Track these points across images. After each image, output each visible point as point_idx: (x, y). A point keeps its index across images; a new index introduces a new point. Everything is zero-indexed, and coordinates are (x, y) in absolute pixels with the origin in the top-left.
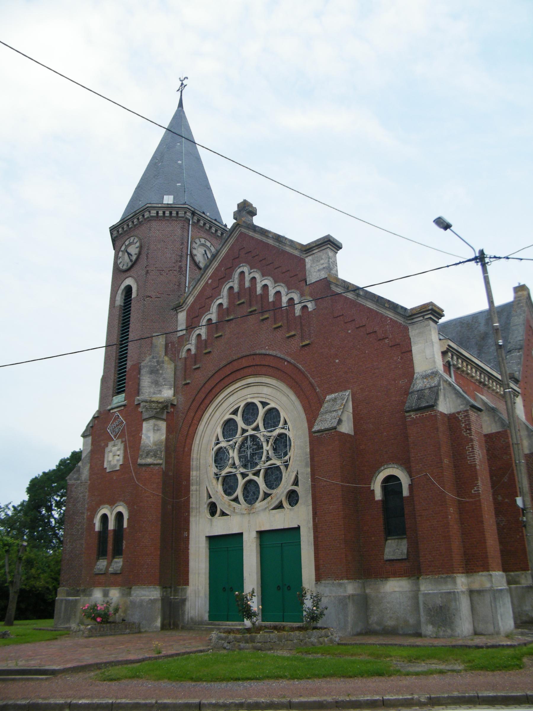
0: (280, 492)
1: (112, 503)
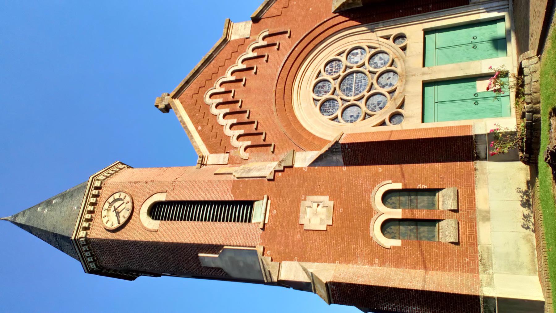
1: (369, 213)
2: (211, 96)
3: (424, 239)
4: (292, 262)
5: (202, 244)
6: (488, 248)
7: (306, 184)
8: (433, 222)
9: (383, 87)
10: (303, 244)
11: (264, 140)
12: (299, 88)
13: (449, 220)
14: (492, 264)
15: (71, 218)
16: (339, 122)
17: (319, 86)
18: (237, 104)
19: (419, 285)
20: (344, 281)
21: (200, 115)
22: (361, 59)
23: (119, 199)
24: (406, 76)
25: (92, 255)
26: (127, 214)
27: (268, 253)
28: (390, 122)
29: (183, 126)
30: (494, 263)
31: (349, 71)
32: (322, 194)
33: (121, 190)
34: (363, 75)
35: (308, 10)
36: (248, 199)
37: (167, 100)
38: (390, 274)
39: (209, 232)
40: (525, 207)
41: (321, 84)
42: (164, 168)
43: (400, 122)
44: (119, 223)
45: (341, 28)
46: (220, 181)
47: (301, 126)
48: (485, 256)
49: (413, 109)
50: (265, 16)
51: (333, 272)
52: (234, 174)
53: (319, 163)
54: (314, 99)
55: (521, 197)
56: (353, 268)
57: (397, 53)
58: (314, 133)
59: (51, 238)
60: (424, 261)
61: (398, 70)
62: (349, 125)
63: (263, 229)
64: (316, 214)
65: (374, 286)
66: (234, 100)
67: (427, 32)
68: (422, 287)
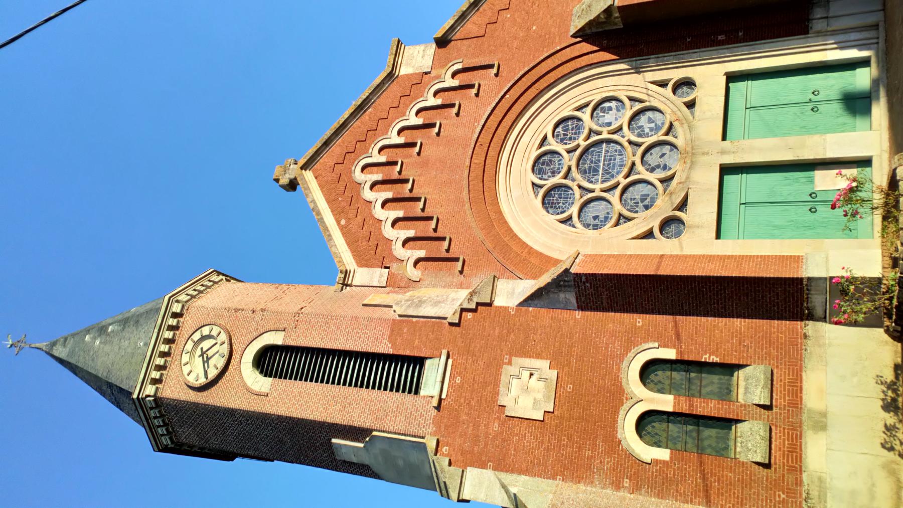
0: (650, 219)
1: (617, 396)
2: (363, 169)
4: (484, 471)
6: (820, 479)
7: (512, 336)
8: (727, 423)
9: (652, 170)
11: (448, 251)
12: (509, 163)
13: (755, 422)
15: (134, 360)
16: (574, 226)
17: (543, 162)
18: (405, 185)
21: (345, 199)
22: (616, 119)
23: (209, 337)
24: (693, 154)
25: (165, 424)
26: (221, 363)
27: (444, 450)
28: (661, 233)
31: (595, 138)
32: (538, 356)
34: (619, 147)
35: (529, 29)
36: (416, 353)
37: (293, 171)
39: (349, 404)
40: (889, 412)
41: (546, 158)
42: (284, 287)
43: (678, 235)
45: (584, 64)
46: (370, 319)
47: (510, 230)
48: (814, 493)
49: (701, 212)
50: (457, 36)
52: (394, 308)
53: (536, 302)
54: (533, 184)
55: (883, 392)
57: (679, 113)
58: (530, 243)
59: (104, 388)
61: (680, 142)
62: (591, 233)
63: (438, 408)
64: (526, 390)
66: (401, 177)
67: (732, 78)
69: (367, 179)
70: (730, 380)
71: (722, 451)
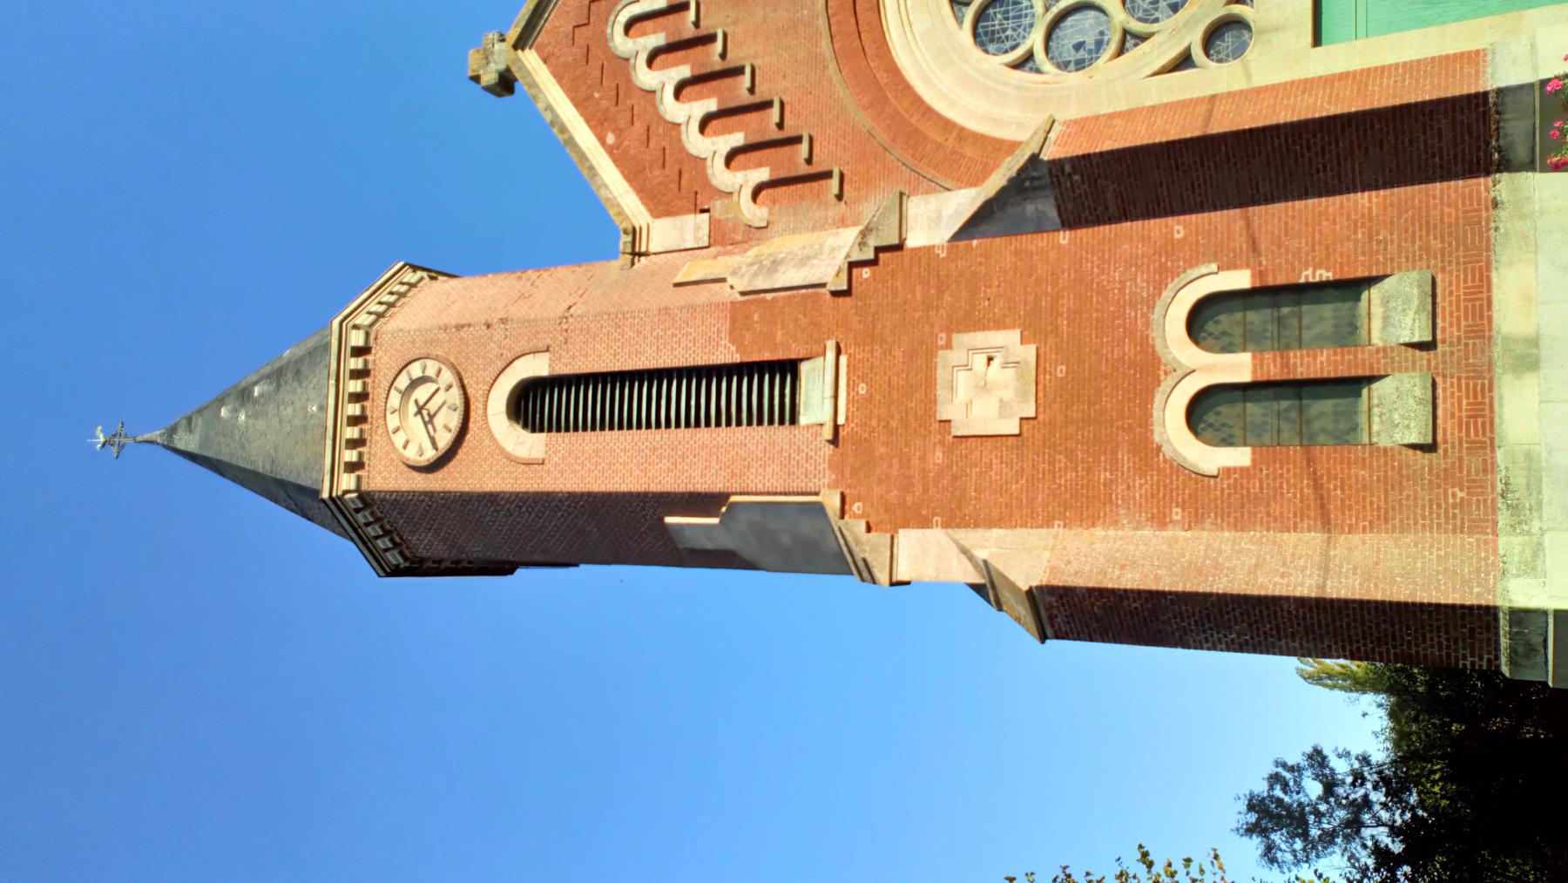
1: (1148, 370)
2: (628, 27)
3: (1321, 438)
4: (928, 531)
5: (668, 494)
6: (1528, 456)
7: (947, 298)
10: (955, 478)
13: (1405, 376)
14: (1540, 504)
15: (309, 438)
16: (1038, 71)
19: (1308, 582)
20: (1080, 582)
26: (455, 421)
27: (855, 507)
28: (1207, 54)
29: (560, 137)
30: (1545, 498)
32: (999, 325)
33: (423, 352)
37: (502, 55)
38: (1220, 552)
39: (683, 457)
43: (1239, 51)
44: (435, 446)
47: (918, 101)
48: (1518, 481)
51: (1047, 555)
52: (730, 281)
53: (983, 228)
56: (1106, 538)
60: (1322, 506)
62: (1074, 78)
63: (835, 441)
64: (984, 387)
65: (1170, 593)
68: (1318, 587)
69: (639, 47)
70: (1354, 309)
71: (1347, 433)
